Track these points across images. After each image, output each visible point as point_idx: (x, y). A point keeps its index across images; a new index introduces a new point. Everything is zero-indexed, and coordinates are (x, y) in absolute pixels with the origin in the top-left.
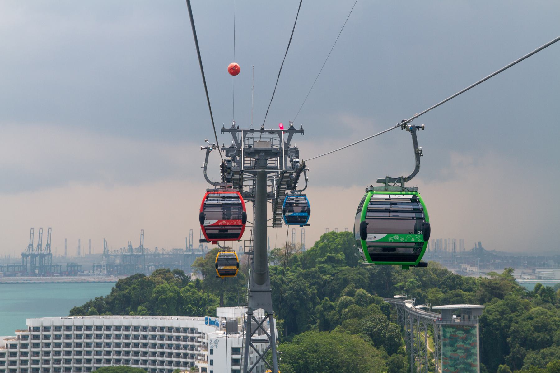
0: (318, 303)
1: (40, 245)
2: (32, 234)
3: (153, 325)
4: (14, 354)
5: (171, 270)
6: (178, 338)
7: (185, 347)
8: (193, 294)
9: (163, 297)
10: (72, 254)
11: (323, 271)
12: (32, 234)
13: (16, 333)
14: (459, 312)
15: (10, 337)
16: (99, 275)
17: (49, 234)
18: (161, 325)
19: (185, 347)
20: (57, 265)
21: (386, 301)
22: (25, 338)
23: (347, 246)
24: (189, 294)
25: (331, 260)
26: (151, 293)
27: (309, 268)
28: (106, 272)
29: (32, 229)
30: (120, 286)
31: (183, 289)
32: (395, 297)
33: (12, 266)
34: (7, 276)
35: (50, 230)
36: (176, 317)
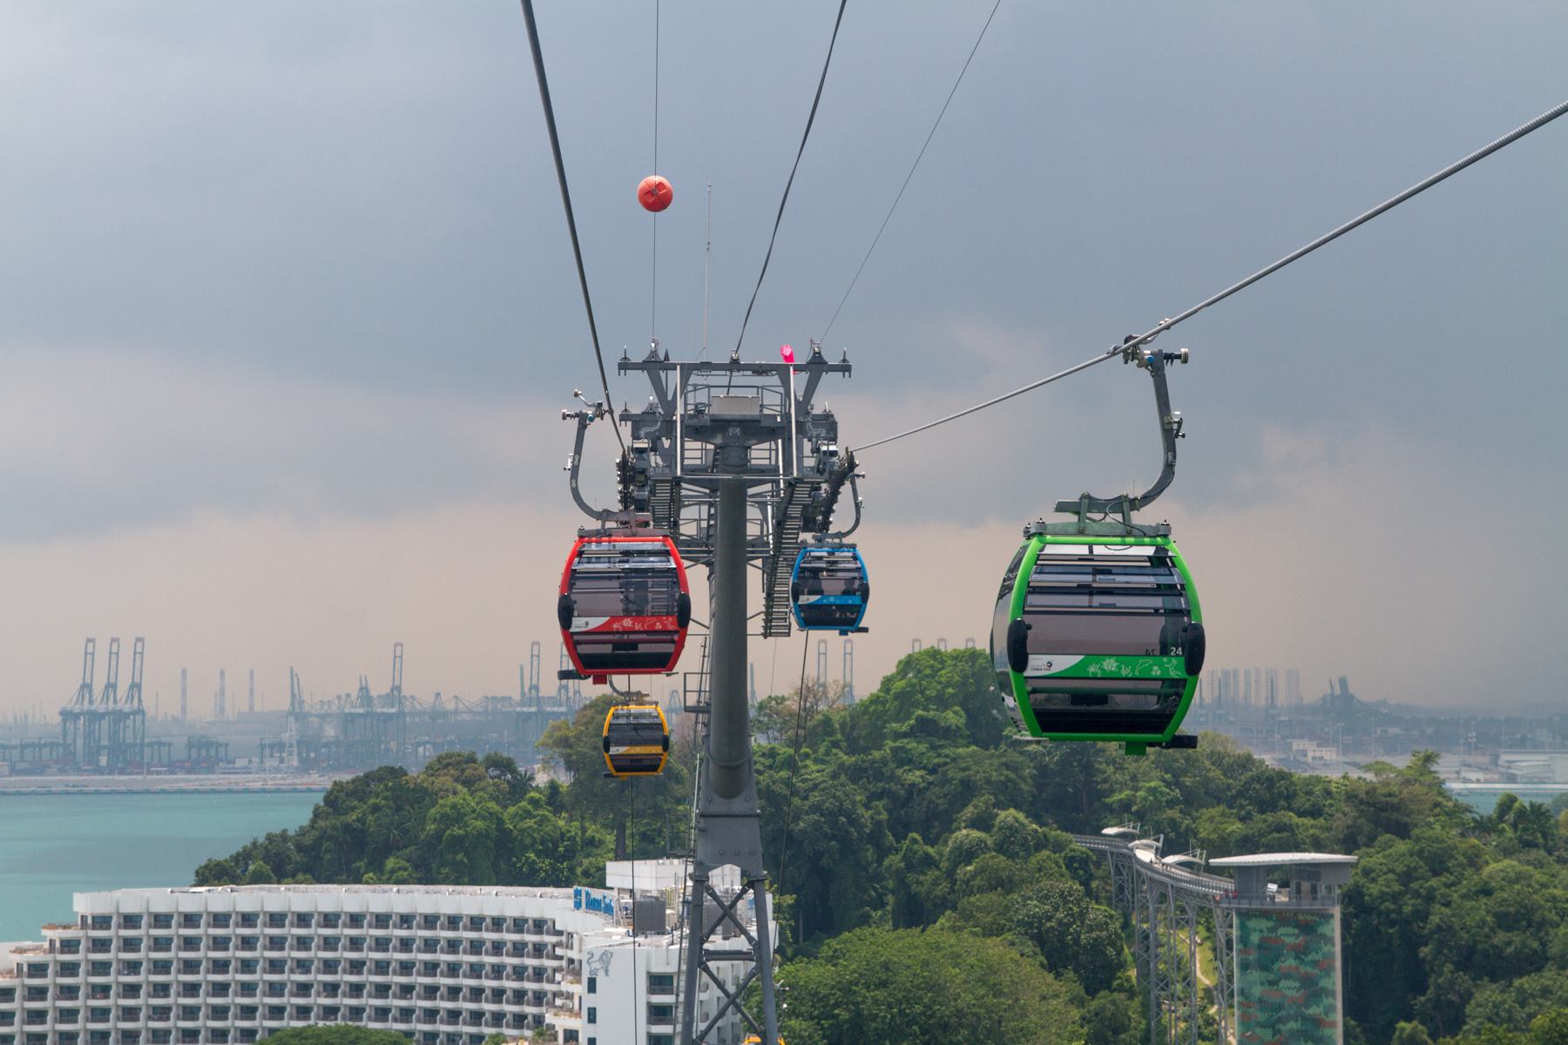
0: (891, 850)
1: (111, 686)
2: (89, 656)
3: (429, 910)
4: (39, 993)
5: (480, 757)
6: (497, 948)
7: (519, 973)
8: (540, 823)
9: (458, 831)
10: (201, 711)
11: (904, 759)
12: (89, 656)
13: (45, 932)
14: (1284, 875)
15: (28, 944)
16: (278, 770)
17: (138, 655)
18: (451, 911)
19: (519, 973)
20: (160, 744)
21: (1079, 845)
22: (69, 946)
23: (972, 689)
24: (530, 823)
25: (926, 728)
26: (422, 821)
27: (866, 750)
28: (295, 763)
29: (89, 640)
30: (335, 800)
31: (512, 810)
32: (1106, 831)
33: (32, 745)
34: (20, 773)
35: (139, 645)
36: (494, 889)
